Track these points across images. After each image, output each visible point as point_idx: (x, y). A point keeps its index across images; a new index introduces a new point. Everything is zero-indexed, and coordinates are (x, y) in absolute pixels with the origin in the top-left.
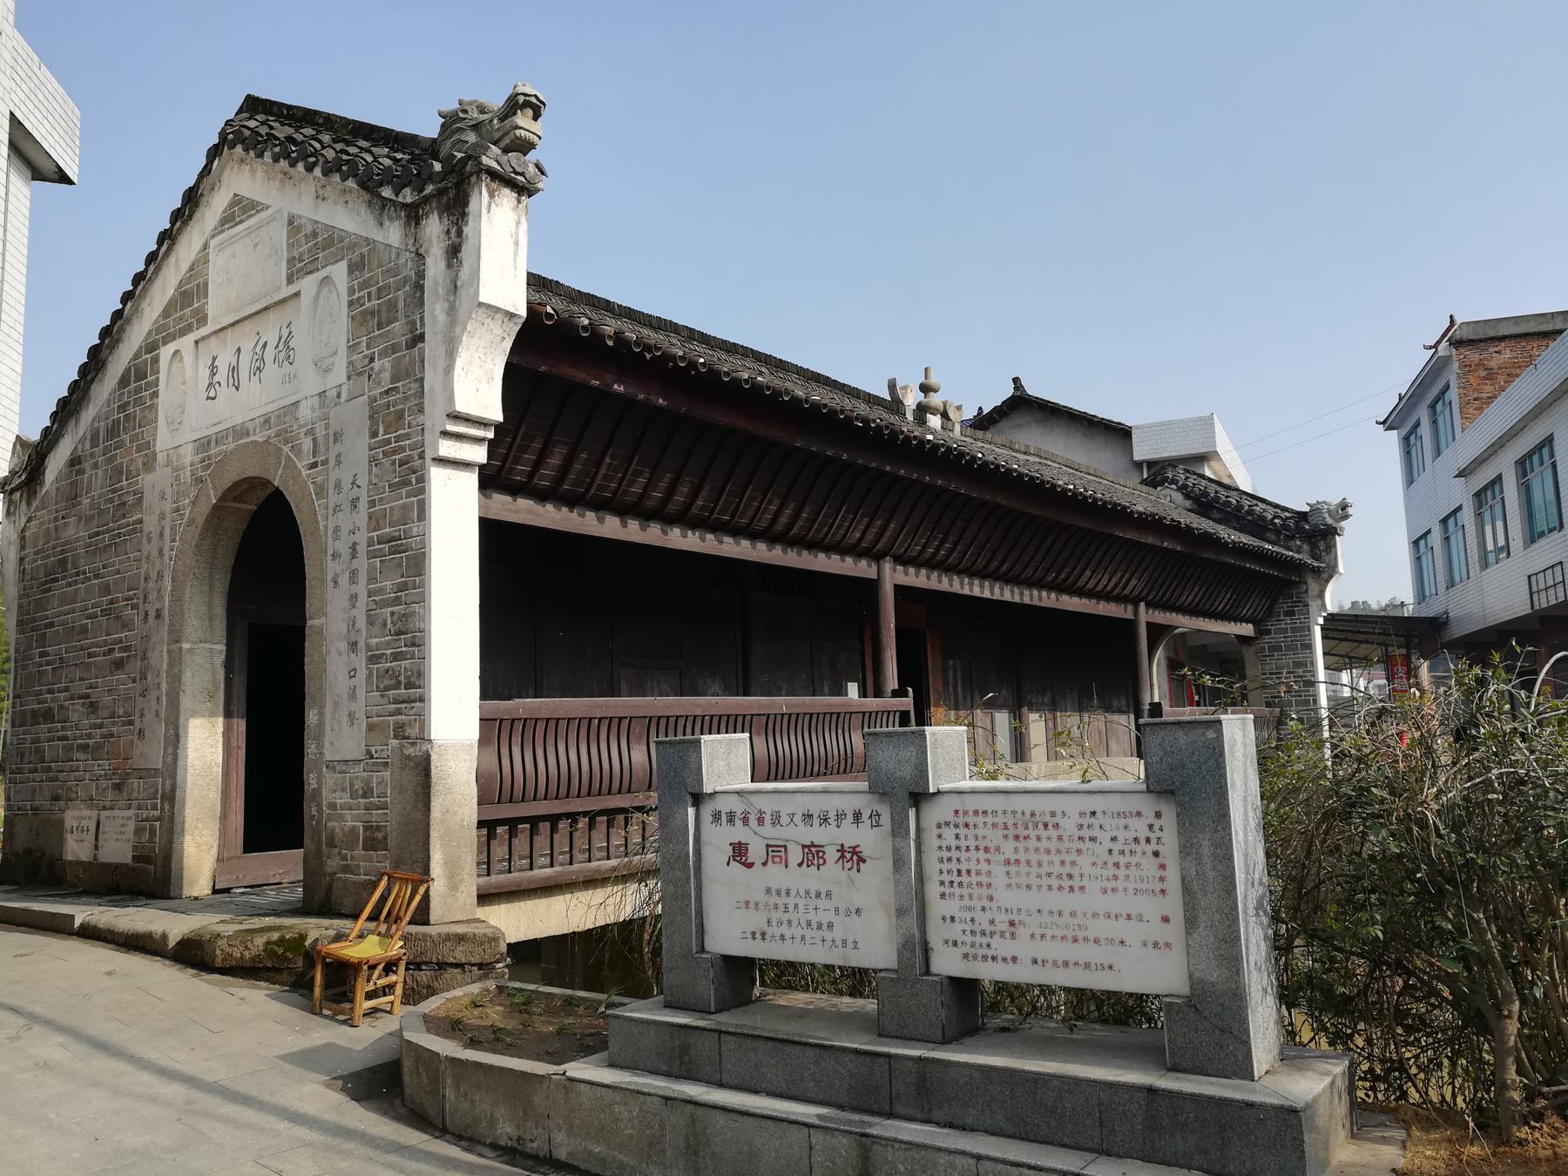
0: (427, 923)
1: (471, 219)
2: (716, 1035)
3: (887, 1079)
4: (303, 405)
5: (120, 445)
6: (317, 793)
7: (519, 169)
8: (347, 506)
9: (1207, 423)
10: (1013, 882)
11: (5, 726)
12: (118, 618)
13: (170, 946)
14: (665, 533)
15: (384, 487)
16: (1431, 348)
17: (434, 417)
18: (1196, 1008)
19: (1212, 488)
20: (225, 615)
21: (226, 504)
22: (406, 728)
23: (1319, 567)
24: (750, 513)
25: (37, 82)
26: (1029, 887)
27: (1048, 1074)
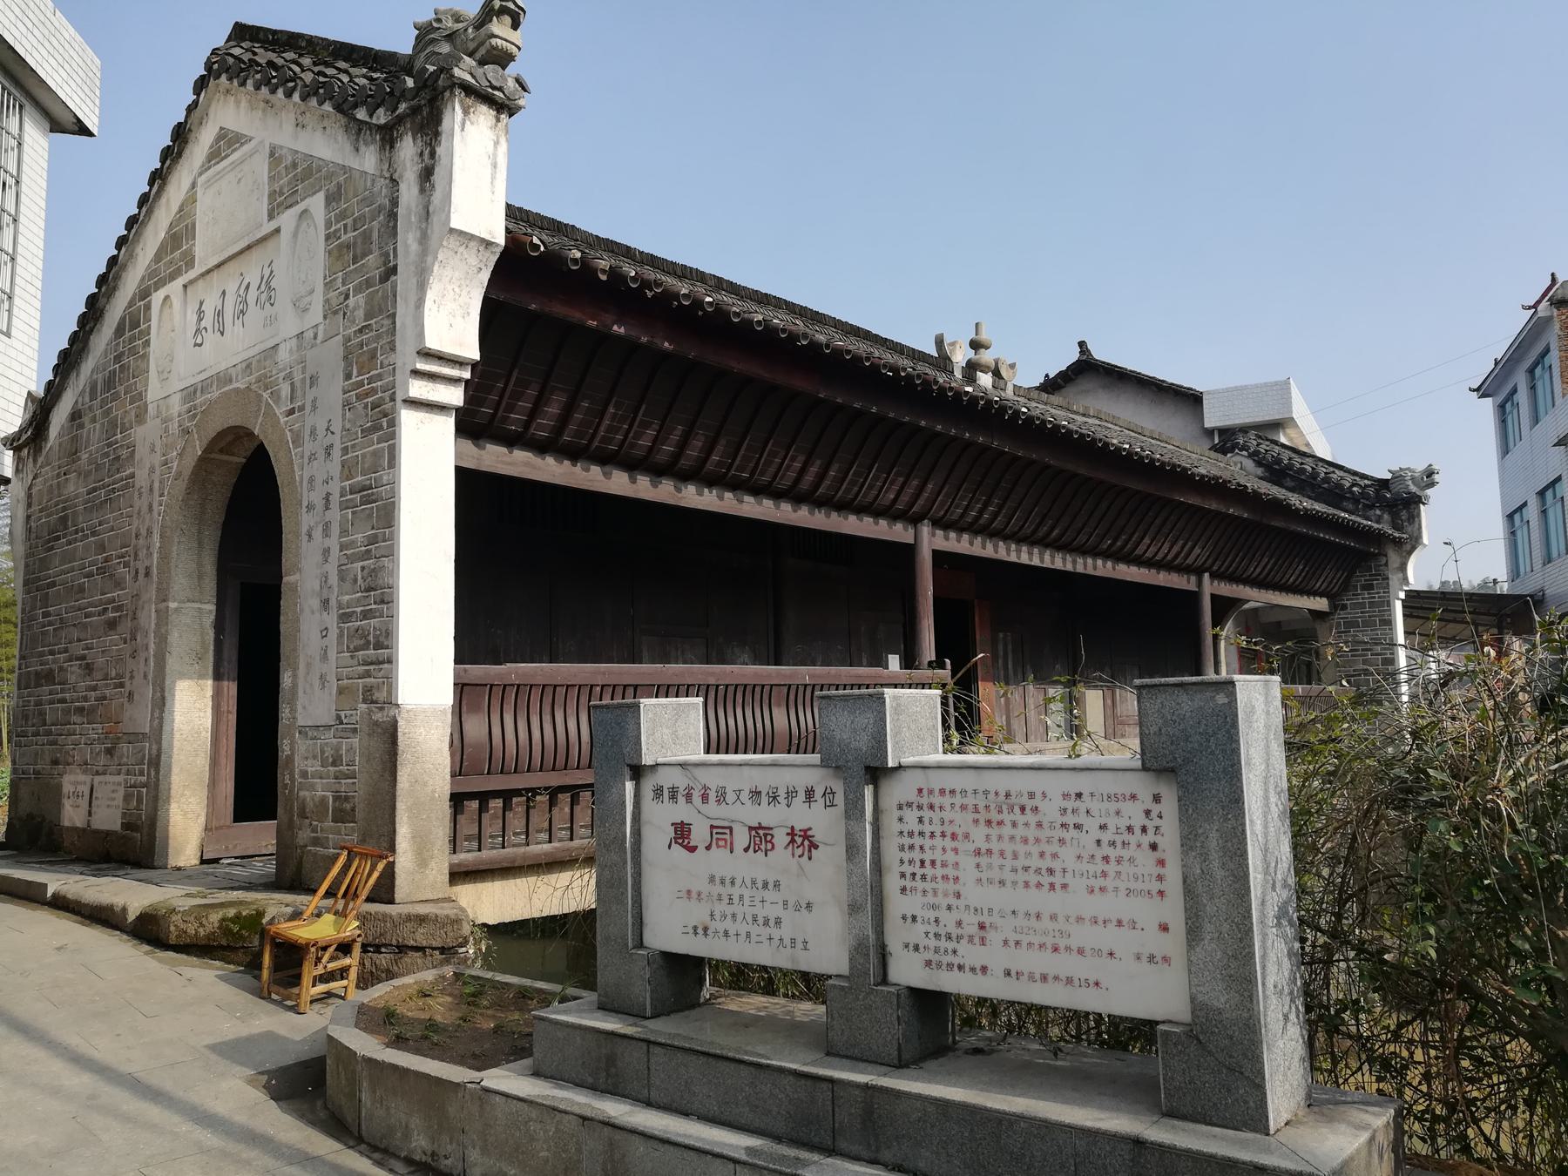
0: (391, 901)
1: (444, 138)
2: (644, 1046)
3: (830, 1108)
4: (282, 346)
5: (116, 397)
6: (290, 759)
7: (495, 83)
8: (321, 454)
9: (1284, 387)
10: (984, 876)
11: (9, 687)
12: (112, 576)
13: (130, 921)
14: (679, 490)
15: (356, 433)
16: (1530, 308)
17: (405, 357)
18: (1198, 1040)
19: (1286, 455)
20: (215, 572)
21: (212, 456)
22: (374, 691)
23: (1400, 538)
24: (772, 470)
25: (52, 29)
26: (1002, 883)
27: (1014, 1114)
